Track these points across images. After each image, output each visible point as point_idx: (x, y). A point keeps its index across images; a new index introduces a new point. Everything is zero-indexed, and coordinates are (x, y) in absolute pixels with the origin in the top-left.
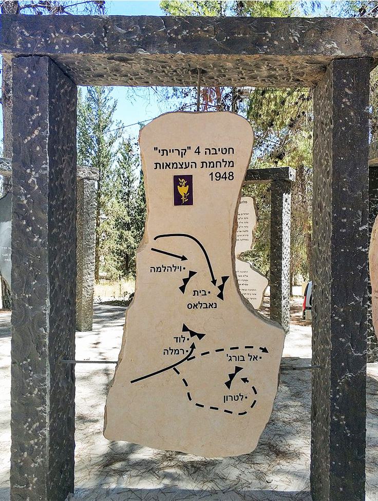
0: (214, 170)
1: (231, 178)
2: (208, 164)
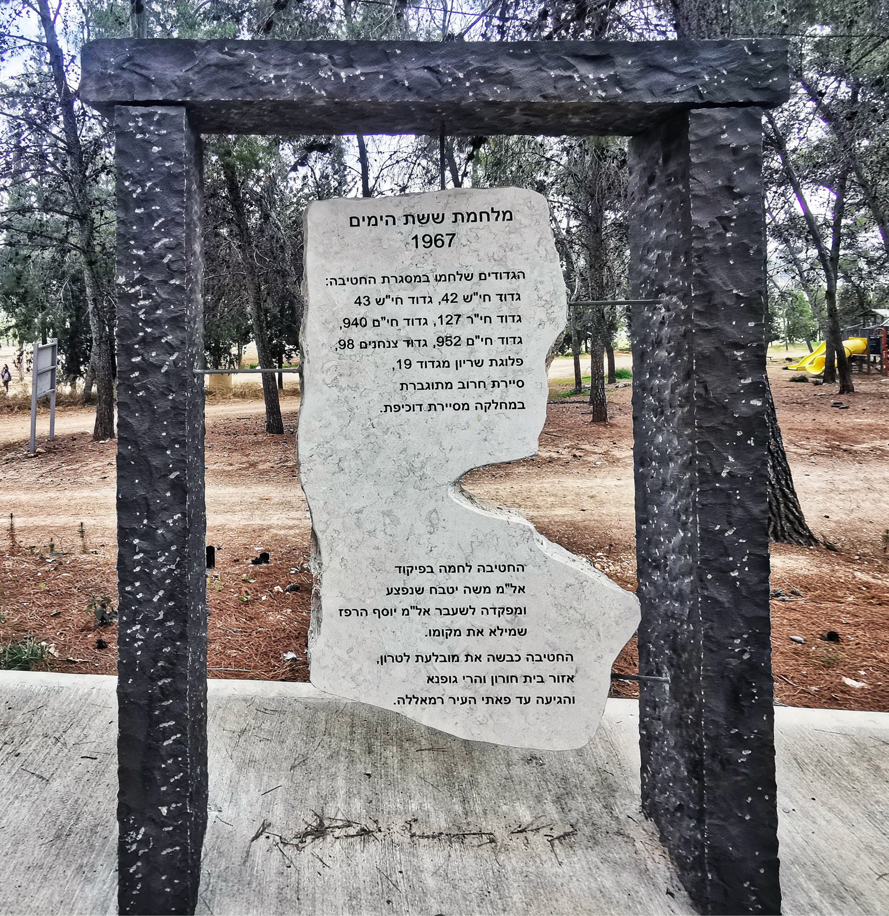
1: (351, 346)
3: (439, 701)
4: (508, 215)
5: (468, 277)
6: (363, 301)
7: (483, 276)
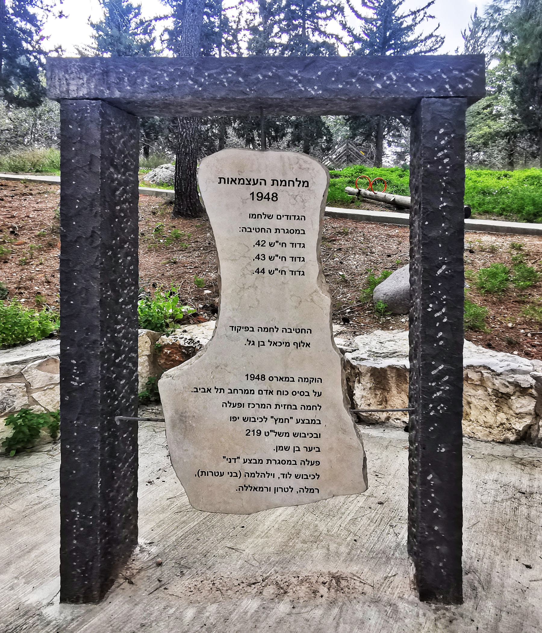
0: (255, 189)
1: (275, 199)
2: (279, 183)
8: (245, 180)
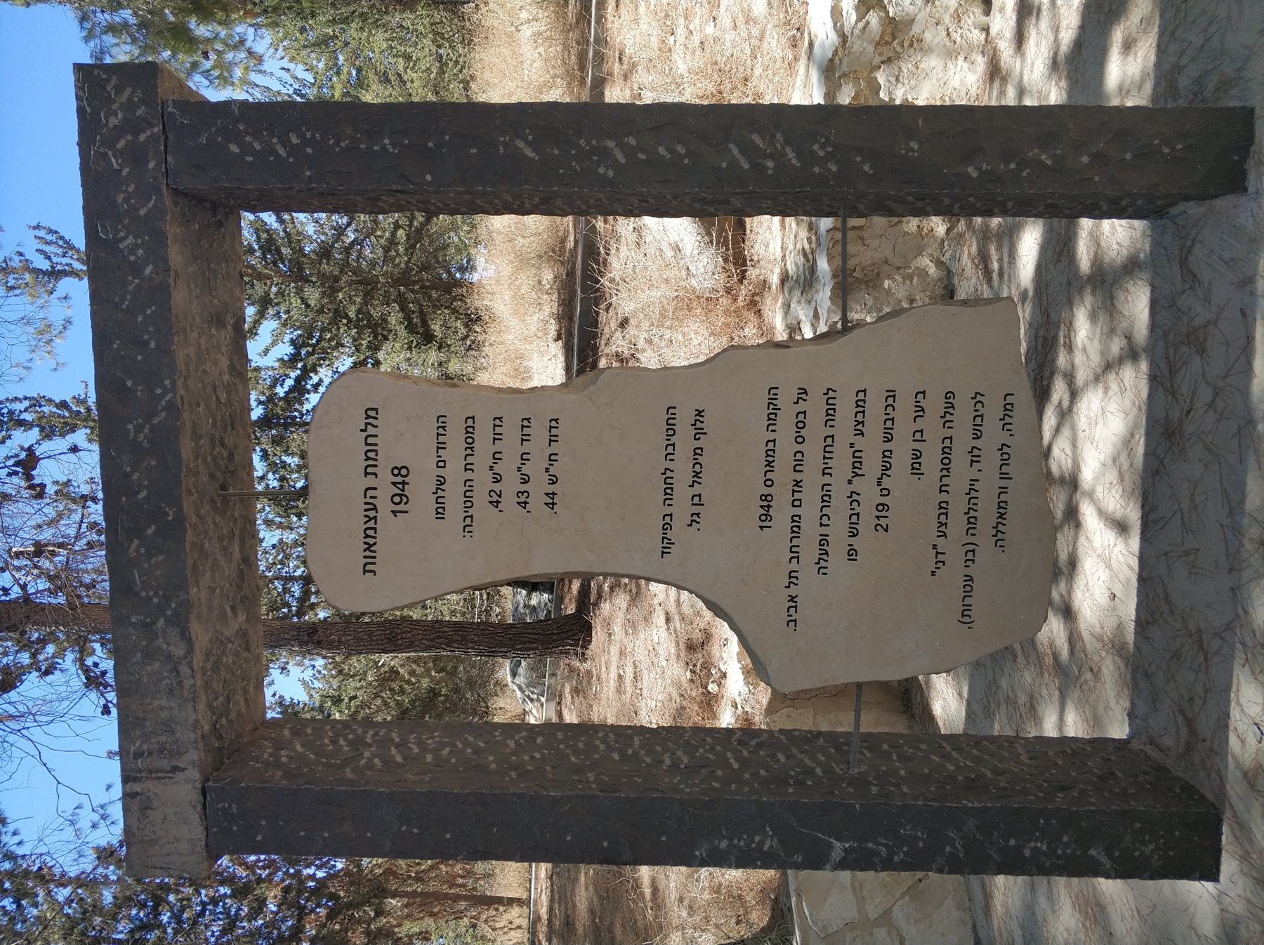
1: (404, 472)
3: (1009, 400)
4: (370, 413)
5: (441, 481)
6: (522, 499)
7: (441, 464)
8: (368, 525)
